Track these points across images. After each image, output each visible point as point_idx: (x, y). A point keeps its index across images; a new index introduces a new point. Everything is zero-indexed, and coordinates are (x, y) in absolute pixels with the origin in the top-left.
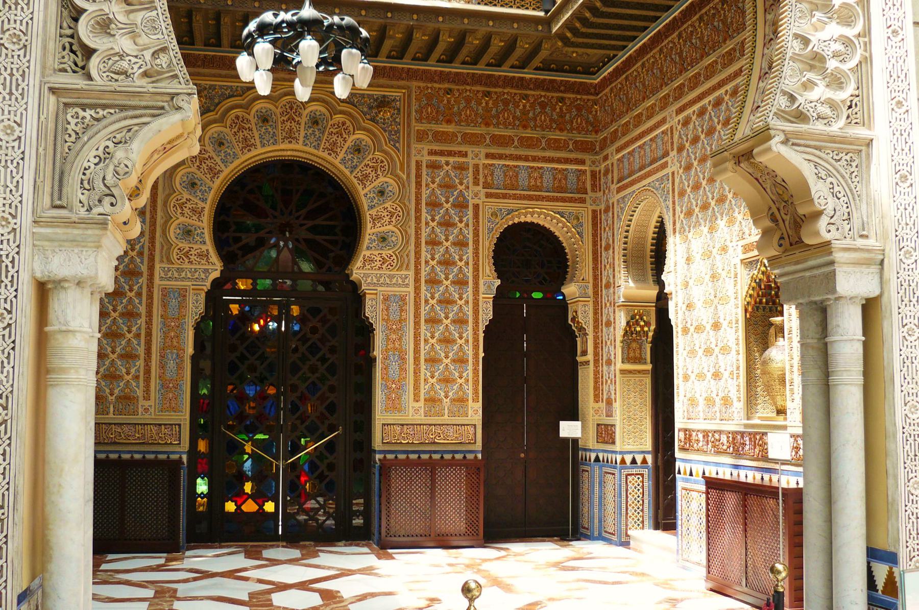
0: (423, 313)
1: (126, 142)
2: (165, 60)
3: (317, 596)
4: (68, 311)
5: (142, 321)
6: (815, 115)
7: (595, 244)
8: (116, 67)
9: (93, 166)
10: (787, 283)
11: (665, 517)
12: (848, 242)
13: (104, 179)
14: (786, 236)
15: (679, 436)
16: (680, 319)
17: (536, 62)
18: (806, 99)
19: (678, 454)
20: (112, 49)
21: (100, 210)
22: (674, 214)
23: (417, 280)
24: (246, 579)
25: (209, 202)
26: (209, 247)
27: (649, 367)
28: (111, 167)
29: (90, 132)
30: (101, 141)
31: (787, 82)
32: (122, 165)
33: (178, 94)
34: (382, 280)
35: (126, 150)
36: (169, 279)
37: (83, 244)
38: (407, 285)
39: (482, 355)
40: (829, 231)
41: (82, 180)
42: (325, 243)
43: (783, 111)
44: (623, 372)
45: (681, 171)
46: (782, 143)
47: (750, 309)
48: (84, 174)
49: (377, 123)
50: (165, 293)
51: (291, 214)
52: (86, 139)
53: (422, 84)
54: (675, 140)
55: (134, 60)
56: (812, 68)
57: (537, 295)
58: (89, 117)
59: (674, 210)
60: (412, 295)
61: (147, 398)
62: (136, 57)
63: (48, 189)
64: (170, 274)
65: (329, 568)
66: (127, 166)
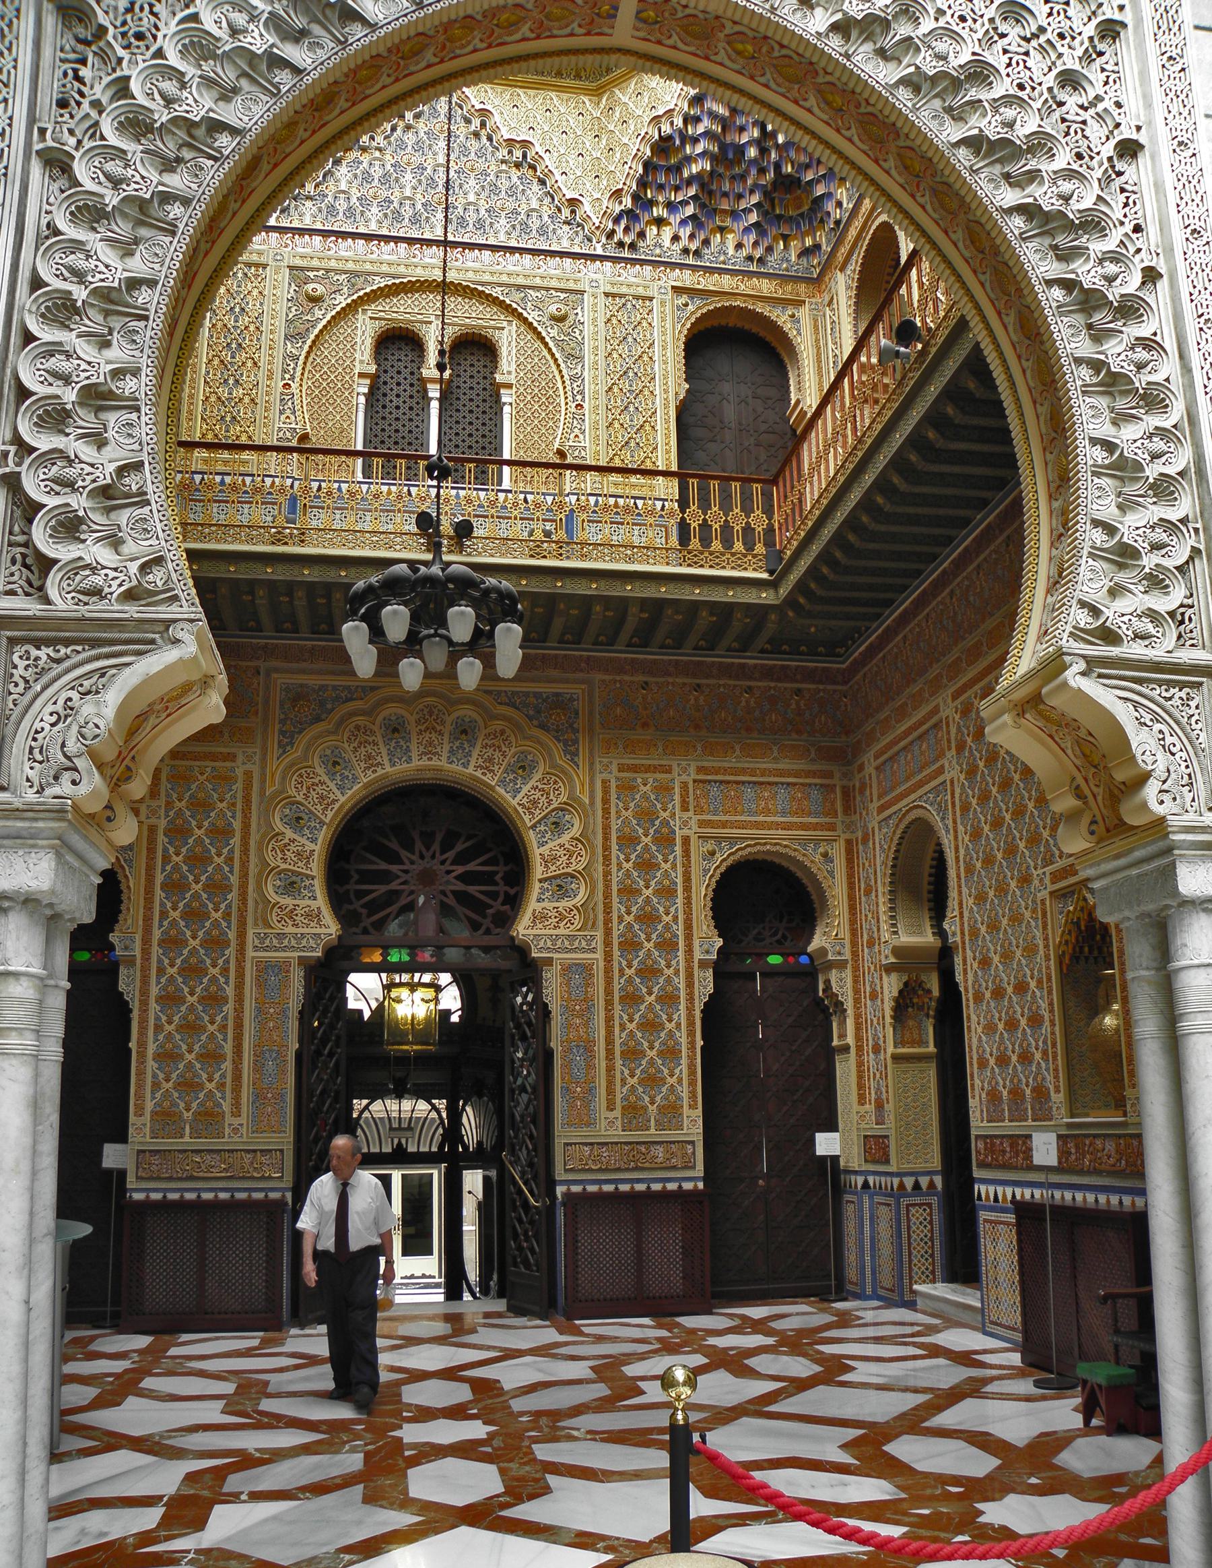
0: (616, 987)
1: (97, 692)
2: (160, 575)
3: (466, 1388)
4: (9, 944)
5: (229, 1008)
6: (1130, 633)
7: (851, 886)
9: (47, 727)
10: (1105, 889)
11: (963, 1266)
12: (1190, 818)
13: (63, 745)
14: (1099, 818)
15: (976, 1146)
16: (970, 983)
17: (761, 641)
18: (1116, 611)
19: (977, 1173)
20: (80, 558)
21: (56, 790)
22: (956, 838)
23: (608, 943)
24: (293, 1355)
25: (320, 841)
26: (321, 902)
27: (931, 1048)
28: (75, 728)
29: (45, 679)
30: (62, 691)
31: (1085, 588)
32: (91, 725)
33: (175, 621)
35: (98, 703)
37: (31, 842)
38: (593, 950)
39: (700, 1043)
40: (1162, 802)
41: (31, 748)
42: (482, 897)
43: (1081, 630)
44: (896, 1058)
45: (962, 777)
47: (1067, 960)
48: (35, 739)
49: (548, 731)
50: (264, 968)
51: (433, 857)
52: (38, 688)
53: (607, 677)
54: (953, 736)
55: (112, 574)
56: (1121, 566)
57: (775, 960)
58: (44, 658)
59: (956, 831)
60: (602, 964)
61: (237, 1113)
62: (115, 570)
64: (267, 942)
65: (489, 1348)
66: (97, 726)
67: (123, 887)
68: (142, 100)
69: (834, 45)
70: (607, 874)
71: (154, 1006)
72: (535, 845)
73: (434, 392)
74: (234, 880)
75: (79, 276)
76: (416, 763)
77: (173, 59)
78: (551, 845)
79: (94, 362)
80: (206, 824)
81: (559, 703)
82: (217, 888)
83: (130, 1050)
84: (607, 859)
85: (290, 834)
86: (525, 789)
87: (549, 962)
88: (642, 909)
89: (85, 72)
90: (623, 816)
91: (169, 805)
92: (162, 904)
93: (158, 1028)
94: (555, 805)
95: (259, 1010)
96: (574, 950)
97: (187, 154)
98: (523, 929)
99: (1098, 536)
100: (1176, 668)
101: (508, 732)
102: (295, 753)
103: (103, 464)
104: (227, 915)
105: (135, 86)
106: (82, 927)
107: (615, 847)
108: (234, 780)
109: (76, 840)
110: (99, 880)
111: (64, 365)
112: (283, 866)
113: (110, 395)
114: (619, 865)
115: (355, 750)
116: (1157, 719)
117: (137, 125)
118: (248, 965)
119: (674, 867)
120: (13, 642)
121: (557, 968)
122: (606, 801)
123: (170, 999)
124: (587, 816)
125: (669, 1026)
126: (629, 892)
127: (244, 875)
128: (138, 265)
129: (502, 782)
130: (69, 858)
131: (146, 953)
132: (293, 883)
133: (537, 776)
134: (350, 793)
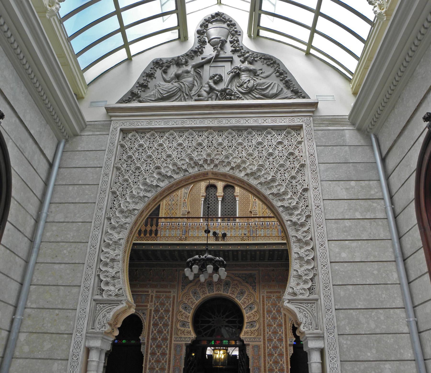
0: (267, 352)
8: (109, 294)
21: (102, 329)
23: (264, 340)
30: (104, 312)
34: (251, 340)
36: (177, 341)
38: (260, 342)
39: (290, 367)
46: (288, 303)
50: (176, 346)
51: (220, 316)
53: (263, 269)
56: (300, 279)
60: (263, 345)
63: (91, 324)
67: (143, 325)
68: (123, 207)
69: (245, 179)
70: (264, 321)
71: (149, 355)
72: (245, 313)
73: (220, 199)
74: (170, 323)
75: (111, 239)
76: (215, 293)
77: (128, 200)
78: (249, 313)
79: (112, 254)
80: (163, 309)
81: (251, 276)
82: (165, 325)
83: (143, 367)
84: (264, 317)
85: (184, 311)
86: (242, 299)
87: (249, 345)
88: (273, 330)
89: (115, 203)
90: (268, 305)
91: (155, 304)
92: (152, 329)
93: (150, 361)
94: (250, 303)
95: (175, 357)
96: (255, 342)
97: (130, 215)
98: (242, 336)
99: (295, 273)
100: (309, 300)
101: (238, 284)
102: (185, 291)
103: (112, 272)
104: (168, 332)
105: (122, 205)
106: (108, 351)
107: (266, 314)
108: (171, 297)
109: (105, 337)
110: (111, 342)
111: (108, 255)
112: (182, 320)
113: (115, 259)
114: (267, 319)
115: (200, 290)
116: (304, 311)
117: (122, 212)
118: (172, 345)
119: (282, 318)
120: (97, 304)
121: (251, 347)
122: (263, 301)
123: (153, 354)
124: (258, 305)
125: (281, 362)
126: (270, 325)
127: (172, 322)
128: (121, 236)
129: (237, 297)
130: (105, 340)
131: (148, 341)
132: (184, 324)
133: (246, 295)
134: (198, 301)
